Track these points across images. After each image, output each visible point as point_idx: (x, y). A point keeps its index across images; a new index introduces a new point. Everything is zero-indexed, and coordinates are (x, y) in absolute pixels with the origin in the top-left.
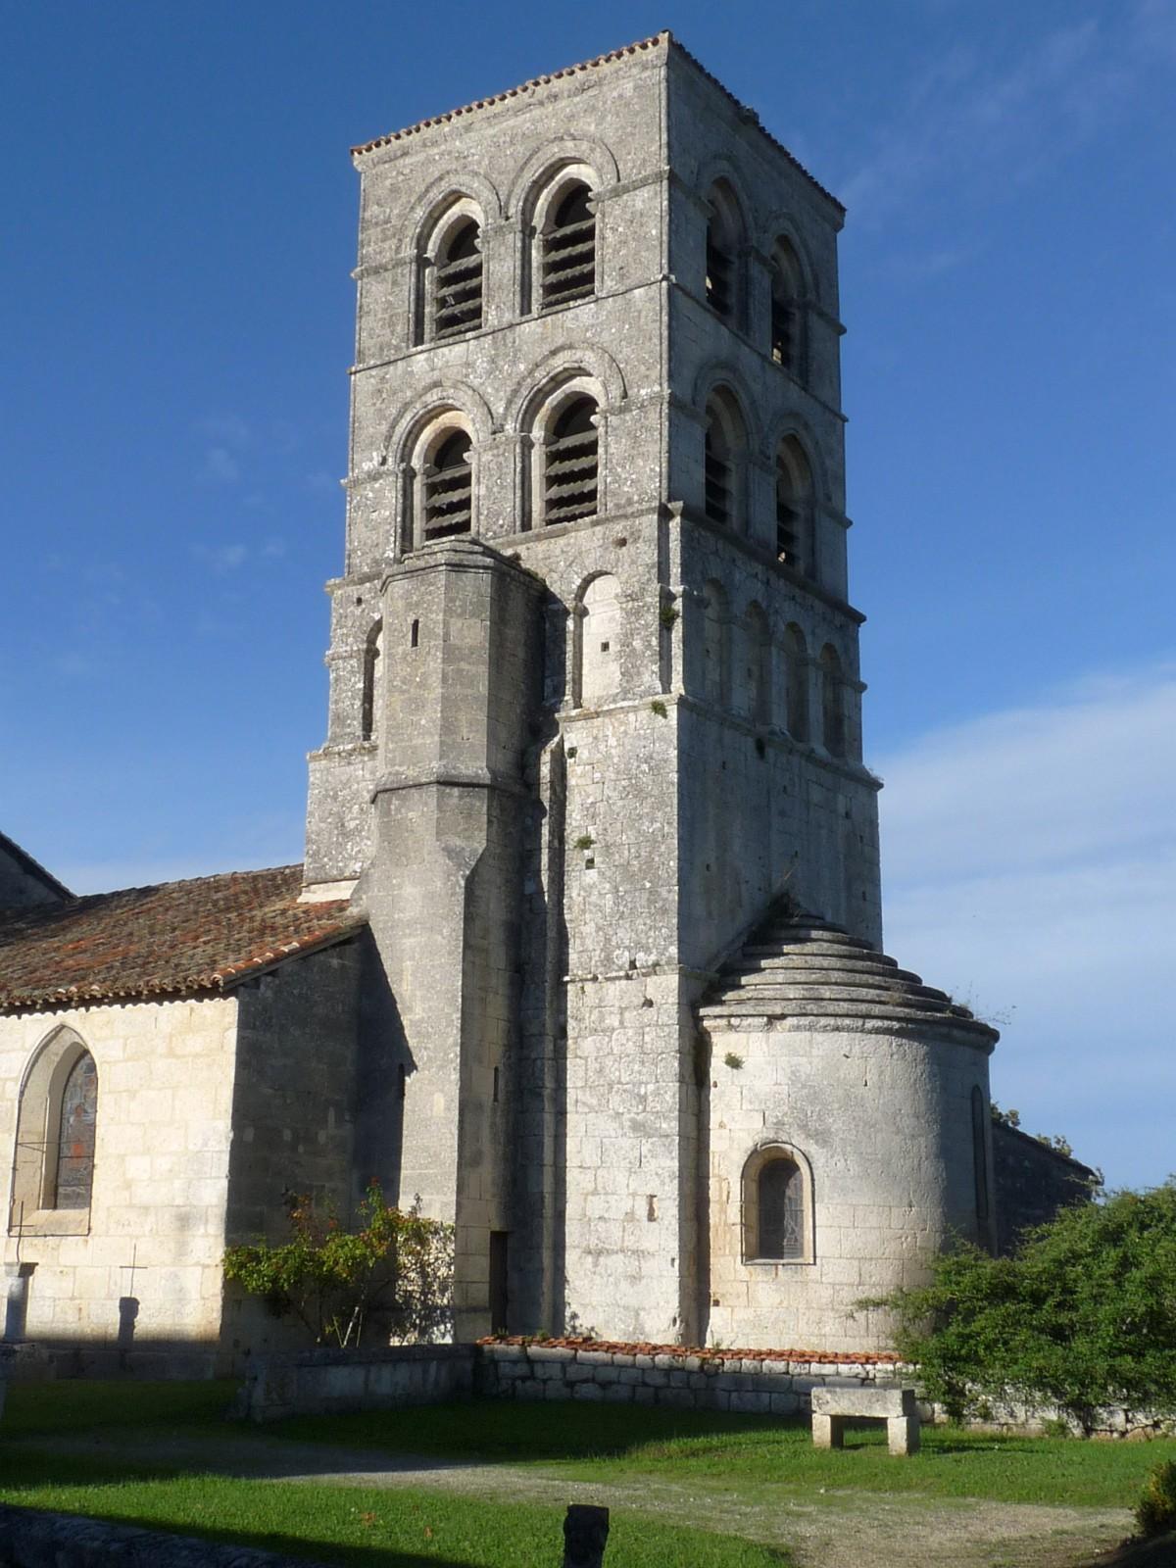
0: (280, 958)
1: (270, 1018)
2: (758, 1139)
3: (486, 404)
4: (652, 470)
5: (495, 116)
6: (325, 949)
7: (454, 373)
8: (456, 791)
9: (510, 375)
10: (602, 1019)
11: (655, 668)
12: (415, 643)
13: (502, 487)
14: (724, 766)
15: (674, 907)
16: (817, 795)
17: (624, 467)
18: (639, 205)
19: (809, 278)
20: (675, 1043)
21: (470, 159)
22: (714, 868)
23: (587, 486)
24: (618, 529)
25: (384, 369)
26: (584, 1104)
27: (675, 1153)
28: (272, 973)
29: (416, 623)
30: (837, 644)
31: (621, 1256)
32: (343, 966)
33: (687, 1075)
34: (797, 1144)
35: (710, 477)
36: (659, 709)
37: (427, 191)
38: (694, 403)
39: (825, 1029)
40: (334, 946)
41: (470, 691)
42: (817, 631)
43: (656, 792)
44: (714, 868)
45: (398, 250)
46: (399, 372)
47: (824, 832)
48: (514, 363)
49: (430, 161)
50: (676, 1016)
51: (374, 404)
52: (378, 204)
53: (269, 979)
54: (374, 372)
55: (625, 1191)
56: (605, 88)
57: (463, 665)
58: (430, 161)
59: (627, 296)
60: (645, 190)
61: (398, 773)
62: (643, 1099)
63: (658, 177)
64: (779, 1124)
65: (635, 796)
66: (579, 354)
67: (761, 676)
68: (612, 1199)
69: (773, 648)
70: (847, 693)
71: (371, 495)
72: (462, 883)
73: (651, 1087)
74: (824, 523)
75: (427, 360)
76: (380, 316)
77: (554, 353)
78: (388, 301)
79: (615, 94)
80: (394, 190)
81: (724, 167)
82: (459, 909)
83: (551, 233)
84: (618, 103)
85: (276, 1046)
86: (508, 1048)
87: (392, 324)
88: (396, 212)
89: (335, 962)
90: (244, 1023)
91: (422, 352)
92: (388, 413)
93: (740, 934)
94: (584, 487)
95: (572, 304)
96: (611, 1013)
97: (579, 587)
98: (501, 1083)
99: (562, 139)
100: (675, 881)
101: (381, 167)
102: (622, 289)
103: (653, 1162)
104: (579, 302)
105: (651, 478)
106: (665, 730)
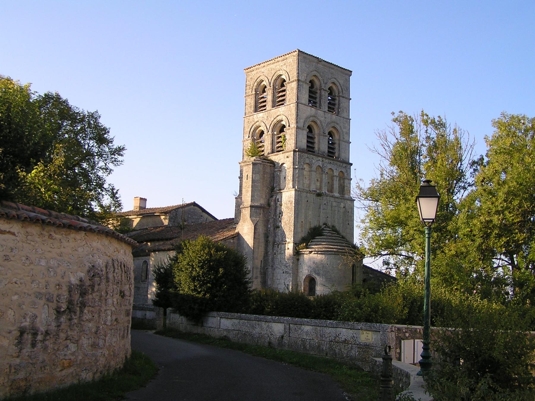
3: (266, 126)
5: (269, 64)
7: (261, 119)
8: (254, 208)
11: (292, 183)
12: (247, 179)
15: (293, 230)
16: (334, 204)
18: (293, 86)
19: (340, 90)
22: (303, 222)
24: (287, 154)
29: (247, 175)
30: (344, 170)
32: (233, 242)
34: (315, 276)
35: (309, 140)
37: (257, 79)
39: (320, 254)
47: (336, 212)
54: (247, 118)
56: (287, 60)
57: (256, 184)
62: (287, 267)
67: (321, 181)
70: (346, 181)
74: (343, 144)
77: (277, 116)
79: (289, 61)
81: (315, 73)
83: (280, 89)
88: (252, 83)
89: (232, 241)
98: (262, 263)
103: (288, 278)
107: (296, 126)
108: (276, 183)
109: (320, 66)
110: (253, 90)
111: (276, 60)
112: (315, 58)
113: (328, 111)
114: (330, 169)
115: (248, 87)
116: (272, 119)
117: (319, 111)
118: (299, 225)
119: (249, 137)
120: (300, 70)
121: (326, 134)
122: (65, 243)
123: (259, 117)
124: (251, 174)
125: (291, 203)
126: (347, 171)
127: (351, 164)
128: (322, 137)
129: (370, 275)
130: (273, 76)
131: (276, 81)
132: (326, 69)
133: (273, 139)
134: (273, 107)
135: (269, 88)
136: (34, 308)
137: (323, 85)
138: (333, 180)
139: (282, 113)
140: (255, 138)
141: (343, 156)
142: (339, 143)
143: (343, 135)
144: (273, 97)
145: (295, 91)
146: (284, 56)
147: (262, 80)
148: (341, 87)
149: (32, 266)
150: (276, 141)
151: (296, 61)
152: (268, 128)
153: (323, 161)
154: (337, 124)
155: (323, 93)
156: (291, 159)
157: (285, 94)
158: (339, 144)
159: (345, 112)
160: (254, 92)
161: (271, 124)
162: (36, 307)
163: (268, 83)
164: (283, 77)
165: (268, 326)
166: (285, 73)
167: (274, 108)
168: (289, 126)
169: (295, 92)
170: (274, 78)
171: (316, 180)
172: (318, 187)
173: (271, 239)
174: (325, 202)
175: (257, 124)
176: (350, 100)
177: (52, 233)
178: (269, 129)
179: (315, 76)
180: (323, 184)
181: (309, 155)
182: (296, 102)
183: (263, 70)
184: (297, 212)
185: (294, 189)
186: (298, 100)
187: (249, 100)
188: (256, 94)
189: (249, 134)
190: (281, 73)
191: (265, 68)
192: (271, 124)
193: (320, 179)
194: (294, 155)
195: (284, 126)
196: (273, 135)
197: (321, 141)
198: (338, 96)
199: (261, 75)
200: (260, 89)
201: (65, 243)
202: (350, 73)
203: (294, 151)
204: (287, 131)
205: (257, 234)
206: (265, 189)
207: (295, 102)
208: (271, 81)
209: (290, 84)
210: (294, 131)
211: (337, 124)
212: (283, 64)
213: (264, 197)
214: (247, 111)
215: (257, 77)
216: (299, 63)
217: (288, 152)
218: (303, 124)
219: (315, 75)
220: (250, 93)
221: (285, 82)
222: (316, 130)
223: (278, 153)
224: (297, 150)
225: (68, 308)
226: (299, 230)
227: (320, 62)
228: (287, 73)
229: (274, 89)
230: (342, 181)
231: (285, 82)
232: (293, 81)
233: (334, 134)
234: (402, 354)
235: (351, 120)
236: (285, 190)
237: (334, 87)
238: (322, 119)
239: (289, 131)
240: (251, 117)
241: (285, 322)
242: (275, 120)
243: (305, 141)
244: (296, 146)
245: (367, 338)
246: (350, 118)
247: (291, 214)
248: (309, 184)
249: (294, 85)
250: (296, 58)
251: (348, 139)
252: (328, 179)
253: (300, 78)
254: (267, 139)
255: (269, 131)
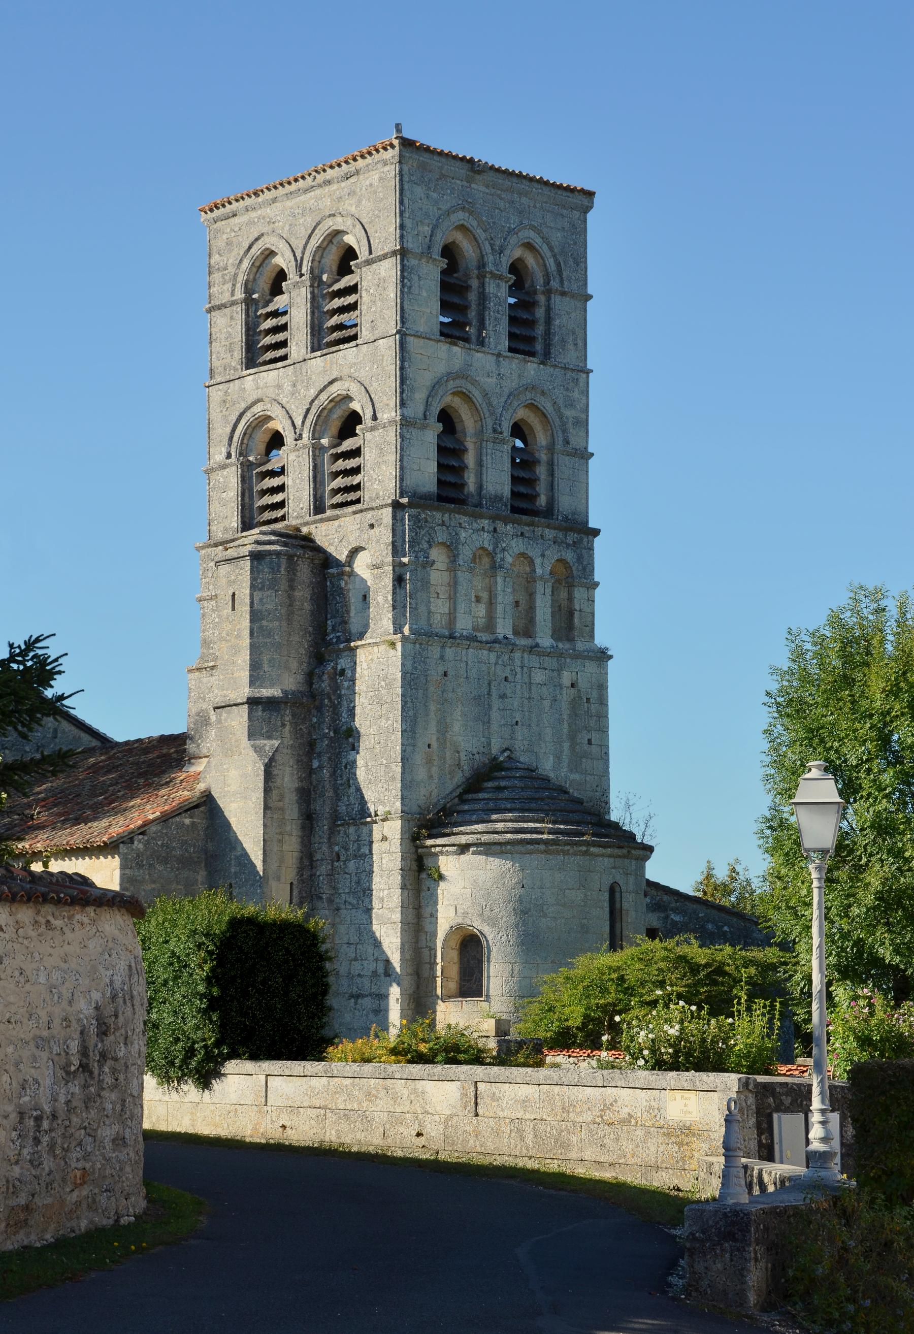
0: (147, 824)
1: (142, 861)
2: (453, 923)
3: (290, 417)
4: (391, 473)
6: (180, 814)
9: (305, 397)
10: (359, 849)
11: (390, 615)
12: (233, 609)
13: (302, 480)
14: (445, 674)
15: (399, 777)
17: (374, 470)
18: (383, 274)
20: (398, 864)
21: (277, 224)
23: (355, 480)
24: (369, 516)
25: (227, 385)
26: (350, 903)
27: (399, 934)
28: (142, 833)
29: (234, 595)
31: (370, 998)
32: (193, 823)
33: (408, 883)
35: (445, 461)
36: (393, 644)
38: (425, 418)
40: (186, 811)
41: (268, 640)
42: (547, 553)
43: (389, 700)
44: (435, 745)
45: (233, 294)
46: (237, 388)
47: (547, 703)
48: (307, 388)
49: (251, 223)
50: (399, 847)
51: (221, 411)
52: (219, 254)
53: (141, 837)
54: (221, 386)
55: (371, 958)
58: (251, 223)
59: (375, 343)
60: (387, 261)
61: (225, 696)
63: (394, 253)
64: (465, 914)
65: (378, 703)
66: (346, 385)
68: (365, 963)
69: (498, 578)
70: (579, 594)
71: (221, 480)
72: (263, 768)
73: (386, 892)
74: (564, 463)
75: (253, 380)
76: (223, 343)
77: (331, 383)
78: (228, 332)
79: (368, 183)
80: (229, 243)
81: (460, 217)
82: (261, 785)
84: (369, 190)
85: (147, 877)
86: (301, 870)
87: (231, 351)
88: (231, 261)
89: (187, 821)
90: (123, 867)
91: (250, 375)
92: (230, 418)
93: (459, 786)
94: (353, 480)
95: (341, 347)
96: (364, 845)
97: (347, 556)
98: (295, 892)
99: (334, 215)
100: (399, 759)
101: (219, 224)
102: (372, 339)
104: (346, 345)
105: (389, 479)
106: (394, 659)
107: (398, 418)
108: (333, 617)
109: (479, 188)
110: (238, 286)
111: (320, 178)
112: (458, 163)
113: (511, 350)
114: (523, 555)
115: (217, 276)
116: (313, 392)
117: (479, 355)
118: (418, 758)
119: (229, 456)
120: (407, 215)
121: (505, 434)
122: (69, 935)
123: (261, 384)
124: (248, 591)
125: (389, 686)
126: (579, 559)
127: (596, 532)
128: (490, 445)
129: (672, 916)
130: (310, 237)
131: (320, 253)
132: (499, 196)
133: (319, 461)
134: (313, 351)
135: (297, 278)
136: (34, 1067)
137: (491, 258)
138: (531, 595)
139: (346, 371)
140: (251, 458)
141: (565, 503)
142: (552, 460)
143: (564, 431)
144: (313, 313)
145: (392, 293)
146: (347, 162)
147: (267, 249)
148: (554, 256)
149: (28, 987)
150: (329, 467)
151: (392, 183)
152: (298, 422)
153: (495, 530)
154: (543, 393)
155: (491, 287)
156: (384, 534)
157: (356, 302)
158: (551, 464)
159: (571, 347)
160: (240, 295)
161: (308, 410)
162: (38, 1065)
163: (293, 263)
164: (349, 239)
165: (415, 1091)
166: (354, 226)
167: (319, 353)
168: (375, 418)
169: (393, 295)
170: (315, 242)
171: (473, 599)
172: (482, 621)
173: (323, 808)
174: (507, 672)
175: (257, 409)
176: (587, 300)
177: (50, 918)
178: (302, 430)
179: (462, 228)
180: (499, 609)
181: (447, 515)
182: (398, 332)
183: (268, 211)
184: (411, 713)
185: (399, 636)
186: (403, 322)
187: (220, 319)
188: (249, 302)
189: (230, 445)
190: (338, 223)
191: (277, 204)
192: (308, 410)
193: (485, 595)
194: (394, 517)
195: (354, 419)
196: (318, 450)
197: (487, 460)
198: (543, 293)
199: (264, 230)
200: (264, 283)
201: (69, 935)
202: (586, 202)
203: (396, 506)
204: (368, 435)
205: (275, 794)
206: (296, 638)
207: (395, 331)
208: (303, 253)
209: (374, 265)
210: (391, 436)
211: (543, 393)
212: (346, 191)
213: (294, 665)
214: (216, 363)
215: (252, 239)
216: (406, 187)
217: (372, 509)
218: (421, 409)
219: (462, 225)
220: (226, 298)
221: (356, 258)
222: (467, 420)
223: (337, 512)
224: (405, 500)
225: (81, 1065)
226: (421, 774)
227: (477, 177)
228: (359, 226)
229: (316, 279)
230: (564, 594)
231: (356, 258)
232: (384, 257)
233: (531, 429)
234: (777, 1147)
235: (591, 375)
236: (368, 640)
237: (531, 261)
238: (490, 382)
239: (376, 433)
240: (231, 384)
241: (462, 1077)
242: (323, 397)
243: (431, 467)
244: (401, 487)
245: (685, 1109)
246: (589, 367)
247: (390, 722)
248: (450, 614)
249: (389, 270)
250: (391, 171)
251: (583, 444)
252: (514, 590)
253: (409, 245)
254: (295, 463)
255: (301, 435)
